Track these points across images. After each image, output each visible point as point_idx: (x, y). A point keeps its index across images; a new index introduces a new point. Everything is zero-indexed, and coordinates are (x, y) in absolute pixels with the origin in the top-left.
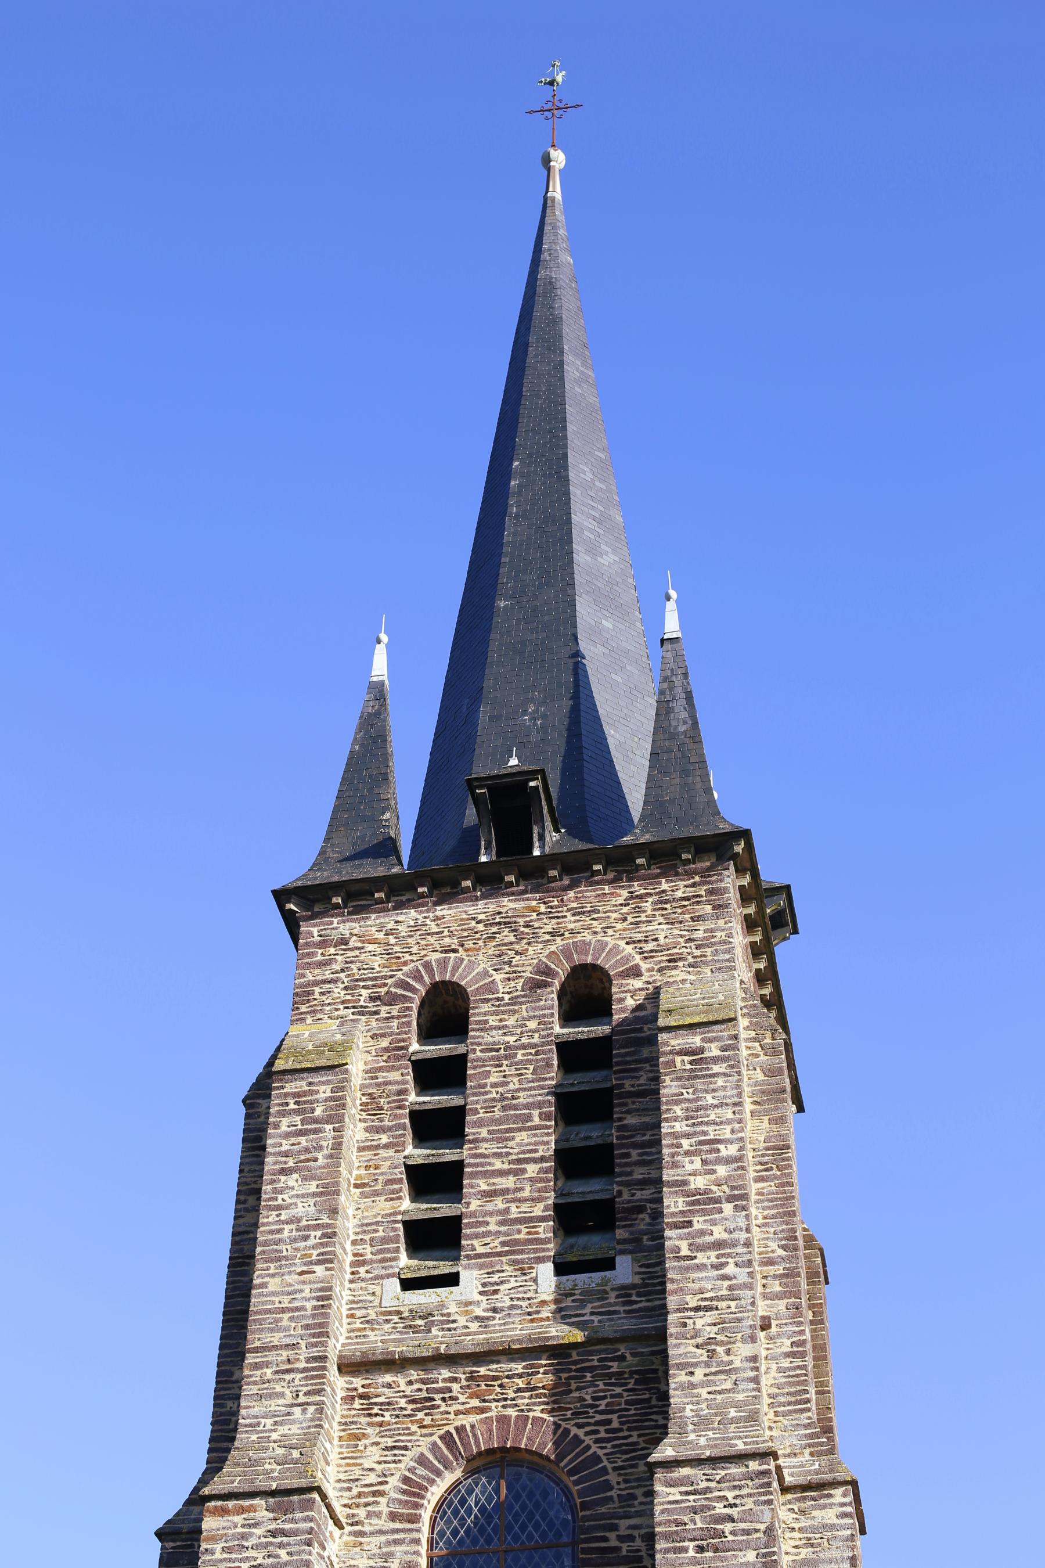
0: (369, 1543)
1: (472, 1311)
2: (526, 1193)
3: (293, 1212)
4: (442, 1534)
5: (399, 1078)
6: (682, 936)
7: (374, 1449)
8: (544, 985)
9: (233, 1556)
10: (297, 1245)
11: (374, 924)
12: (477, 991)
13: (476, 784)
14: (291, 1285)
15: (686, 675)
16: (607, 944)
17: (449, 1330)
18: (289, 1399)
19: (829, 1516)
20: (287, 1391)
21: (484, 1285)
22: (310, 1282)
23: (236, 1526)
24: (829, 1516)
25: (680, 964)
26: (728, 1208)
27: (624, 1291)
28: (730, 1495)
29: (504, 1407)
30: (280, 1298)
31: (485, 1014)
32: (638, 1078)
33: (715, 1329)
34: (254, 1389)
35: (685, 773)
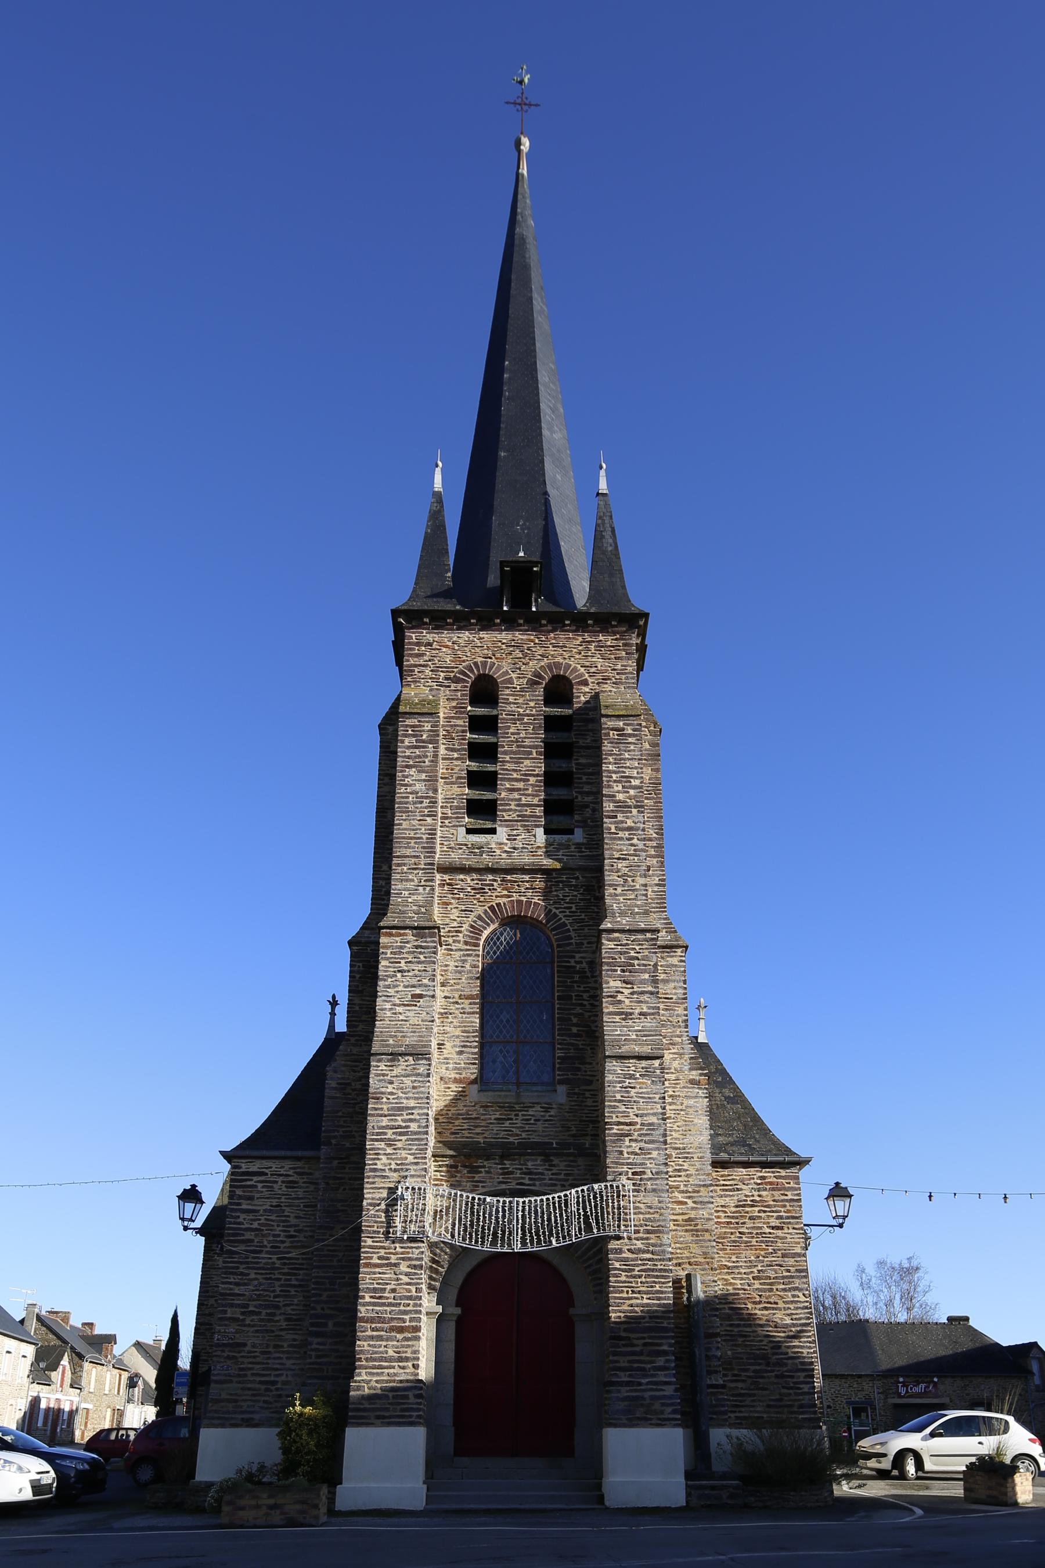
0: (454, 955)
1: (503, 848)
2: (530, 792)
3: (414, 788)
4: (488, 953)
5: (463, 724)
6: (610, 667)
7: (455, 910)
8: (539, 683)
9: (397, 956)
10: (417, 806)
11: (446, 637)
12: (503, 682)
13: (505, 564)
14: (415, 826)
15: (611, 517)
16: (571, 665)
17: (492, 856)
18: (416, 882)
19: (675, 961)
20: (415, 879)
21: (509, 835)
22: (425, 825)
23: (397, 942)
24: (675, 961)
25: (609, 682)
26: (635, 811)
27: (578, 845)
28: (637, 948)
29: (519, 896)
30: (409, 832)
31: (507, 695)
32: (586, 739)
33: (627, 869)
34: (398, 876)
35: (611, 575)
